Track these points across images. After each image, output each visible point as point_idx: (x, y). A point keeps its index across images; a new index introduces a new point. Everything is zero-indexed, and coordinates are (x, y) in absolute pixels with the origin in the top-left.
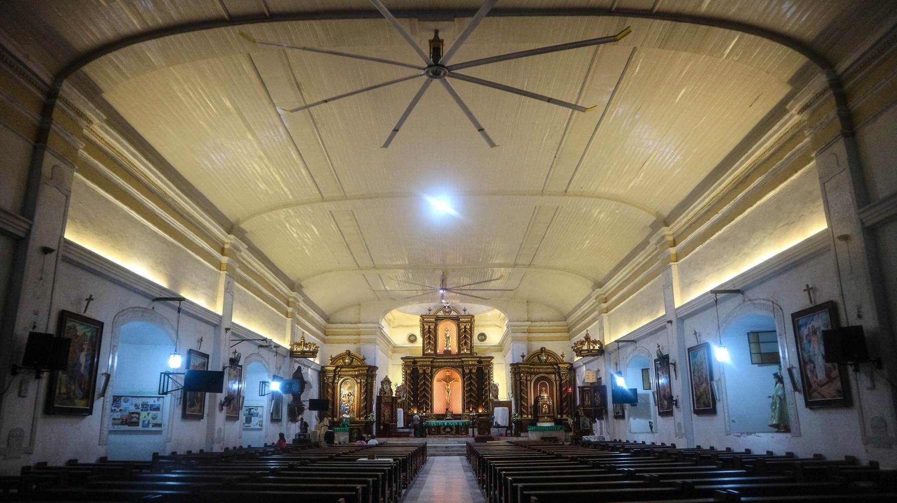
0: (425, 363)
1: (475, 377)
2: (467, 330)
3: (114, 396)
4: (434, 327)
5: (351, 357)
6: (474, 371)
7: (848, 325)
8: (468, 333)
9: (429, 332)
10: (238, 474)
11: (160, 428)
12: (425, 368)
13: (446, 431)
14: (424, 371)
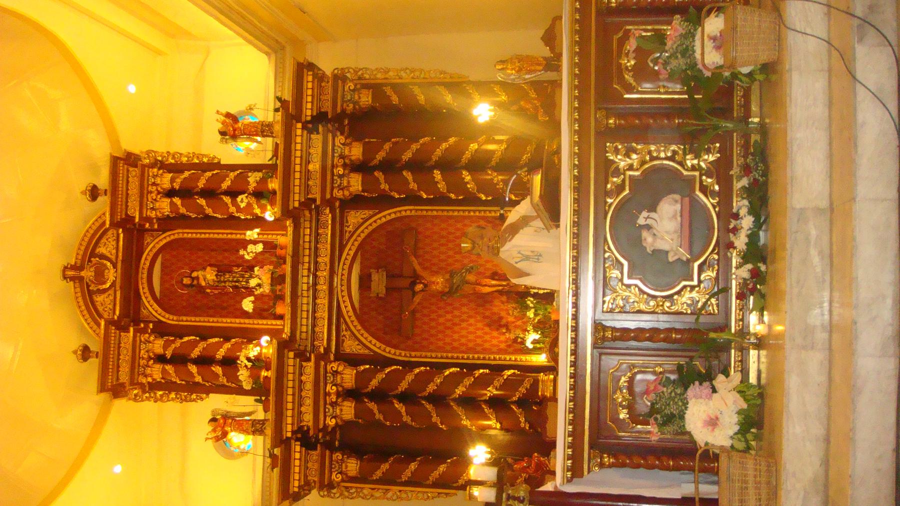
1: (387, 146)
2: (177, 186)
3: (559, 291)
9: (179, 360)
10: (627, 349)
11: (555, 73)
12: (332, 389)
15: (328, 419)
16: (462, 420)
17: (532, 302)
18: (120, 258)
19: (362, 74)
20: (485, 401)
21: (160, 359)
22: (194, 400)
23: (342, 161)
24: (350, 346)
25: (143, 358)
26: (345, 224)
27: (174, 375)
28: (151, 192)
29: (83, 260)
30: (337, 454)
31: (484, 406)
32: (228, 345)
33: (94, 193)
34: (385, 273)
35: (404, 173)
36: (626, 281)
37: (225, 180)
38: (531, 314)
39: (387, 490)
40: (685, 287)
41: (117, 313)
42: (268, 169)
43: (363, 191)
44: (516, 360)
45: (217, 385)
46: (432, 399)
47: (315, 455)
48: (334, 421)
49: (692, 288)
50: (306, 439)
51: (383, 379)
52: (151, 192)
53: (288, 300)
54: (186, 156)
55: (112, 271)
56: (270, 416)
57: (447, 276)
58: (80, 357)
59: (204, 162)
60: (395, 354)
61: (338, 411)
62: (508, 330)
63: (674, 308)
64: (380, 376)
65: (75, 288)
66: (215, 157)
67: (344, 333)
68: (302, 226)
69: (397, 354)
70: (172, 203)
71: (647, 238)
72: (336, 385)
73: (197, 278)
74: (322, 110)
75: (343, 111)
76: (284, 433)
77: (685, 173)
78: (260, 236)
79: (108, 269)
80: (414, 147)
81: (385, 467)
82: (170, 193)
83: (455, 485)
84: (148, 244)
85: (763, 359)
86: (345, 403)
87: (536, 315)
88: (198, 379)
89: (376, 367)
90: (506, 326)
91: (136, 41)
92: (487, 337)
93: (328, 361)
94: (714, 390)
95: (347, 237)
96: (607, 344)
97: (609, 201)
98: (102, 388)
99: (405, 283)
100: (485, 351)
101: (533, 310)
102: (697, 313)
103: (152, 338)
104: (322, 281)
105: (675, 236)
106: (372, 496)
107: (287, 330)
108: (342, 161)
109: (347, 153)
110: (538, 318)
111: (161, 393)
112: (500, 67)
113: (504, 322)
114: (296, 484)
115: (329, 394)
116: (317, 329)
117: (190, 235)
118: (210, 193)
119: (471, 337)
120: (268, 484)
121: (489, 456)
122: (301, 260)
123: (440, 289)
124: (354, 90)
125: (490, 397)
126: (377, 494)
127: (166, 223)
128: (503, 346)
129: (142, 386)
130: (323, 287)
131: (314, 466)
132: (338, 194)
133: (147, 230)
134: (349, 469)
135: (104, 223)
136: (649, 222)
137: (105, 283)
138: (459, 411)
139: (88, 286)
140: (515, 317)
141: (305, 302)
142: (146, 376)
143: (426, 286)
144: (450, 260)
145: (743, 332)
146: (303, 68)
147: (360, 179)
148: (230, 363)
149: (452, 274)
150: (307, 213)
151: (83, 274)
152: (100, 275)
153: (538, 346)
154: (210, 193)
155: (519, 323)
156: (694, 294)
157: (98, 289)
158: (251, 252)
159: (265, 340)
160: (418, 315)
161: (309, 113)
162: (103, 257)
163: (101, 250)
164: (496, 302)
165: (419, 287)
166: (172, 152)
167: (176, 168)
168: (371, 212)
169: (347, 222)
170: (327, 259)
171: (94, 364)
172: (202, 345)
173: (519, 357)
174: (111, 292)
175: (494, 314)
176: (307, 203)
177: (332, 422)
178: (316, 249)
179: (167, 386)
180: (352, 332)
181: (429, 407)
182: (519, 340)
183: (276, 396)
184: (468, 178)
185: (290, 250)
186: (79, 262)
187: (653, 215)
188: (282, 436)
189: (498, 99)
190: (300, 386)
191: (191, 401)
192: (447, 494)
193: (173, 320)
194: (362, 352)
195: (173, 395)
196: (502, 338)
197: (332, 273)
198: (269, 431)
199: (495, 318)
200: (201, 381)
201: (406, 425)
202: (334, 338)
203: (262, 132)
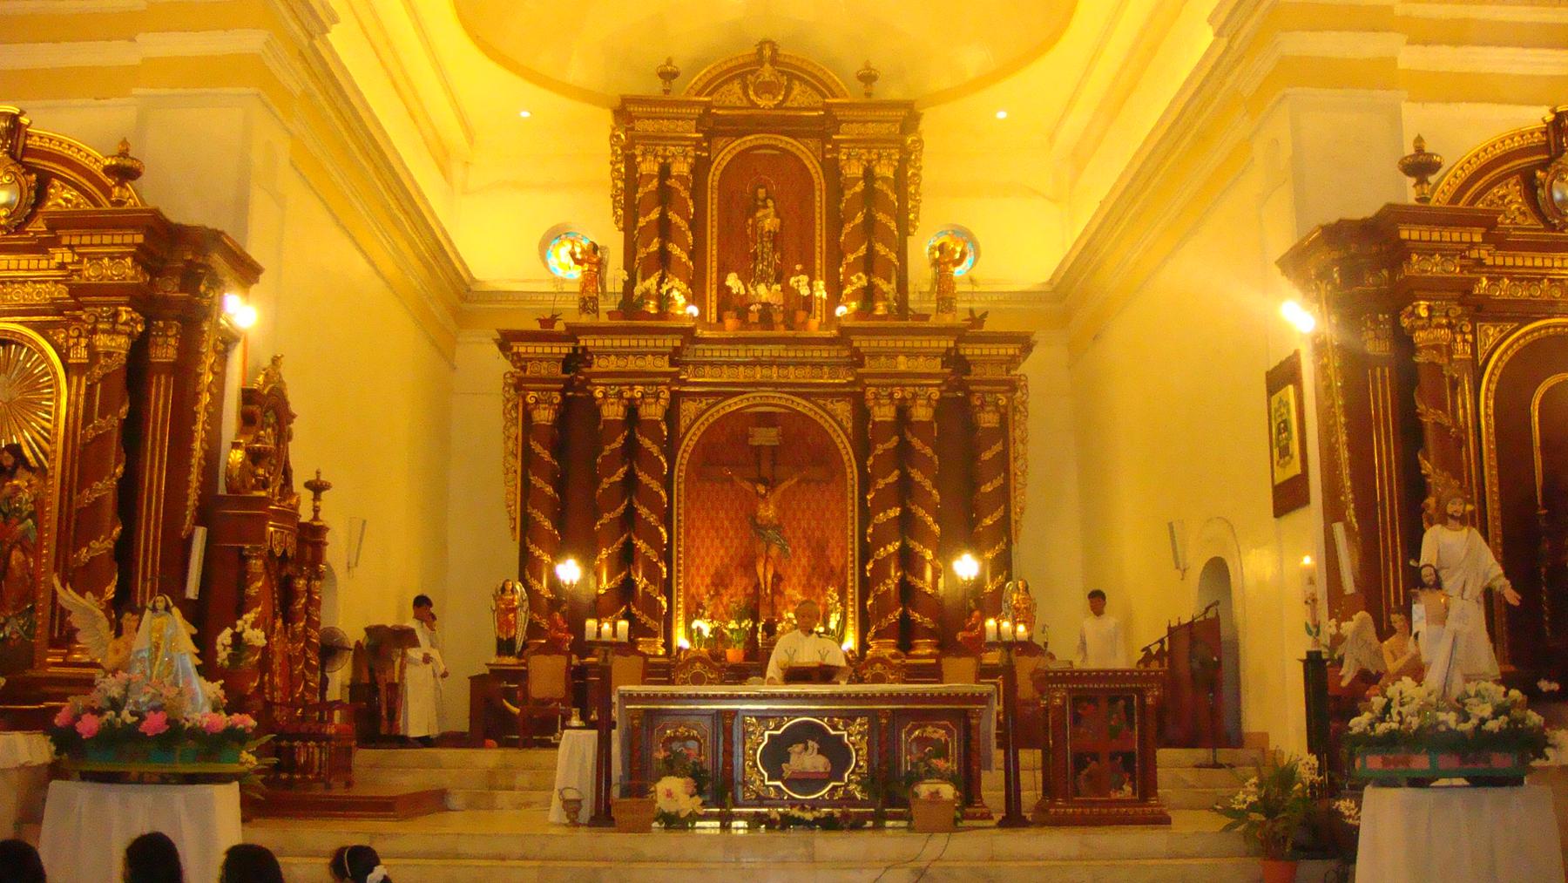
0: (633, 364)
1: (928, 451)
2: (878, 185)
4: (694, 170)
5: (29, 169)
7: (1015, 636)
9: (665, 196)
13: (788, 769)
14: (632, 410)
15: (602, 388)
16: (608, 549)
17: (746, 626)
18: (788, 113)
19: (1019, 411)
20: (629, 574)
21: (665, 172)
22: (615, 213)
23: (909, 396)
24: (689, 408)
25: (665, 150)
26: (835, 400)
27: (646, 190)
28: (869, 152)
29: (782, 64)
30: (559, 397)
31: (624, 573)
32: (684, 257)
33: (868, 78)
34: (778, 443)
35: (896, 472)
36: (767, 733)
37: (886, 247)
38: (733, 625)
39: (516, 456)
40: (763, 775)
41: (720, 112)
42: (902, 308)
43: (875, 424)
44: (678, 609)
45: (635, 243)
46: (631, 512)
47: (557, 370)
48: (600, 395)
49: (763, 781)
50: (576, 361)
51: (651, 453)
52: (869, 152)
53: (742, 334)
54: (917, 192)
55: (771, 104)
56: (604, 320)
57: (775, 522)
58: (663, 69)
59: (908, 214)
60: (681, 464)
61: (612, 400)
62: (712, 597)
63: (747, 769)
64: (655, 450)
65: (749, 55)
66: (915, 227)
67: (704, 402)
68: (831, 348)
69: (682, 467)
70: (858, 180)
71: (798, 748)
72: (643, 396)
73: (766, 207)
74: (972, 367)
75: (972, 393)
76: (584, 337)
77: (766, 742)
78: (819, 301)
79: (774, 98)
80: (928, 484)
81: (546, 455)
82: (869, 175)
83: (528, 540)
84: (806, 145)
85: (713, 831)
86: (621, 408)
87: (732, 631)
88: (642, 222)
89: (665, 442)
90: (717, 593)
91: (1062, 116)
92: (702, 571)
93: (669, 386)
94: (692, 796)
95: (821, 402)
96: (720, 721)
97: (826, 719)
98: (626, 100)
99: (766, 470)
100: (687, 569)
101: (737, 627)
102: (745, 784)
103: (690, 160)
104: (766, 372)
105: (800, 768)
106: (509, 437)
107: (707, 334)
108: (909, 396)
109: (919, 402)
110: (728, 633)
111: (623, 170)
112: (1020, 586)
113: (723, 591)
114: (522, 350)
115: (632, 390)
116: (707, 368)
117: (818, 199)
118: (870, 226)
119: (703, 552)
120: (511, 298)
121: (568, 583)
122: (790, 347)
123: (759, 514)
124: (997, 405)
125: (634, 581)
126: (510, 444)
127: (832, 169)
128: (693, 590)
129: (631, 144)
130: (759, 374)
131: (544, 369)
132: (870, 392)
133: (823, 147)
134: (542, 411)
135: (834, 96)
136: (810, 750)
137: (756, 93)
138: (616, 546)
139: (752, 72)
140: (727, 605)
141: (740, 353)
142: (644, 155)
143: (763, 497)
144: (794, 524)
145: (733, 817)
146: (1025, 344)
147: (889, 419)
148: (663, 261)
149: (778, 528)
150: (846, 353)
151: (767, 66)
152: (767, 88)
153: (695, 635)
154: (870, 227)
155: (721, 610)
156: (758, 783)
157: (747, 87)
158: (800, 284)
159: (694, 310)
160: (727, 486)
161: (968, 352)
162: (789, 90)
163: (797, 88)
164: (745, 581)
165: (761, 489)
166: (922, 172)
167: (901, 182)
168: (850, 431)
169: (837, 401)
170: (792, 379)
171: (655, 88)
172: (684, 225)
173: (681, 612)
174: (745, 103)
175: (731, 580)
176: (857, 359)
177: (598, 394)
178: (804, 364)
179: (631, 180)
180: (706, 411)
181: (621, 509)
182: (701, 611)
183: (628, 327)
184: (891, 549)
185: (803, 334)
186: (781, 59)
187: (816, 751)
188: (580, 334)
189: (988, 581)
190: (639, 353)
191: (614, 207)
192: (514, 528)
193: (713, 181)
194: (683, 424)
195: (620, 184)
196: (703, 590)
197: (776, 385)
198: (585, 320)
199: (727, 581)
200: (640, 224)
201: (598, 482)
202: (698, 389)
203: (942, 299)
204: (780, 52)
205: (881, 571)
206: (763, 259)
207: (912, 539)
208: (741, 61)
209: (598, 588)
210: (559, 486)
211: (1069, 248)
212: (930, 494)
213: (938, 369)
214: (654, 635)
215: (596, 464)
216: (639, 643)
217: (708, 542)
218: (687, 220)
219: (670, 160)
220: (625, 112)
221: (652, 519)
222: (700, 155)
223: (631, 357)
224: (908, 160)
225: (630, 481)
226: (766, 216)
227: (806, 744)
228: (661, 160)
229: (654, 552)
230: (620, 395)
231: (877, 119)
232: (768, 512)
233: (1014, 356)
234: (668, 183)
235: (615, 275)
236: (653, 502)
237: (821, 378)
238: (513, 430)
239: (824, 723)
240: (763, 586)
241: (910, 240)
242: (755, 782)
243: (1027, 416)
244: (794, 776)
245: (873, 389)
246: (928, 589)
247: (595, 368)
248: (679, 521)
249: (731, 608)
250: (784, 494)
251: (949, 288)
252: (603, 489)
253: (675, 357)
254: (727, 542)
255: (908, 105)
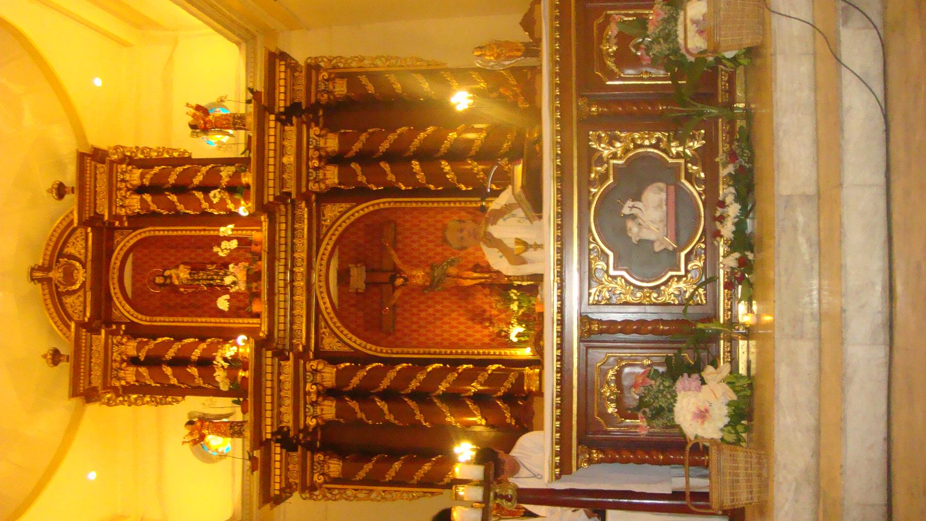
1: (363, 137)
6: (332, 143)
8: (165, 175)
9: (154, 362)
11: (534, 59)
12: (311, 388)
14: (328, 393)
15: (308, 419)
17: (516, 295)
20: (469, 397)
21: (134, 361)
22: (170, 403)
23: (317, 153)
24: (330, 344)
25: (116, 361)
28: (120, 189)
29: (51, 260)
30: (319, 455)
32: (204, 346)
33: (61, 191)
36: (612, 272)
38: (514, 307)
39: (371, 490)
40: (672, 277)
41: (88, 314)
43: (340, 184)
45: (193, 388)
47: (296, 456)
48: (314, 420)
49: (680, 278)
51: (365, 377)
52: (120, 189)
53: (264, 296)
55: (82, 271)
56: (249, 417)
58: (50, 361)
62: (492, 323)
63: (662, 299)
64: (362, 374)
65: (43, 290)
66: (185, 151)
67: (324, 330)
71: (633, 229)
72: (315, 384)
73: (170, 277)
75: (318, 102)
78: (235, 232)
80: (392, 137)
82: (140, 190)
84: (119, 243)
85: (753, 350)
86: (326, 402)
87: (520, 307)
88: (174, 381)
89: (356, 364)
90: (490, 320)
92: (470, 332)
94: (703, 382)
95: (324, 230)
96: (593, 337)
97: (593, 190)
98: (74, 393)
99: (384, 278)
101: (516, 303)
102: (684, 304)
103: (125, 340)
104: (299, 277)
105: (662, 225)
106: (355, 497)
110: (521, 311)
111: (135, 396)
113: (487, 315)
114: (277, 486)
115: (309, 393)
124: (327, 80)
125: (475, 393)
127: (137, 221)
128: (487, 340)
129: (115, 389)
131: (295, 468)
132: (313, 187)
133: (118, 228)
135: (72, 222)
136: (634, 211)
137: (74, 284)
138: (445, 408)
139: (57, 287)
142: (119, 379)
145: (732, 323)
146: (275, 58)
148: (206, 363)
150: (282, 207)
151: (51, 275)
152: (69, 276)
153: (523, 339)
155: (503, 316)
156: (682, 285)
158: (225, 249)
160: (399, 310)
161: (282, 104)
162: (71, 257)
163: (70, 250)
165: (399, 281)
166: (141, 146)
167: (145, 164)
168: (348, 206)
169: (324, 216)
171: (65, 368)
172: (177, 346)
173: (508, 352)
174: (81, 293)
176: (283, 197)
177: (312, 423)
178: (293, 244)
179: (142, 389)
180: (331, 330)
181: (412, 404)
182: (503, 334)
185: (265, 246)
186: (47, 263)
191: (166, 404)
192: (432, 493)
195: (147, 398)
196: (486, 332)
197: (310, 268)
199: (478, 311)
201: (388, 423)
203: (234, 124)
204: (40, 264)
205: (465, 177)
206: (212, 279)
207: (439, 151)
208: (48, 296)
209: (481, 425)
210: (394, 455)
211: (210, 30)
212: (400, 135)
213: (294, 128)
214: (521, 376)
215: (374, 425)
216: (529, 390)
217: (446, 327)
218: (173, 343)
219: (125, 357)
220: (90, 396)
221: (421, 377)
222: (124, 331)
223: (282, 394)
224: (130, 157)
225: (390, 395)
226: (178, 277)
227: (626, 216)
228: (124, 365)
229: (449, 376)
230: (314, 404)
231: (93, 180)
232: (419, 276)
233: (287, 66)
234: (142, 359)
235: (222, 406)
236: (406, 376)
237: (303, 229)
238: (349, 493)
239: (597, 191)
240: (483, 280)
241: (194, 157)
242: (679, 289)
243: (341, 57)
244: (672, 232)
245: (311, 184)
246: (482, 136)
247: (291, 425)
248: (424, 353)
249: (502, 307)
250: (405, 262)
251: (225, 119)
252: (395, 419)
253: (280, 355)
254: (446, 311)
255: (81, 157)
